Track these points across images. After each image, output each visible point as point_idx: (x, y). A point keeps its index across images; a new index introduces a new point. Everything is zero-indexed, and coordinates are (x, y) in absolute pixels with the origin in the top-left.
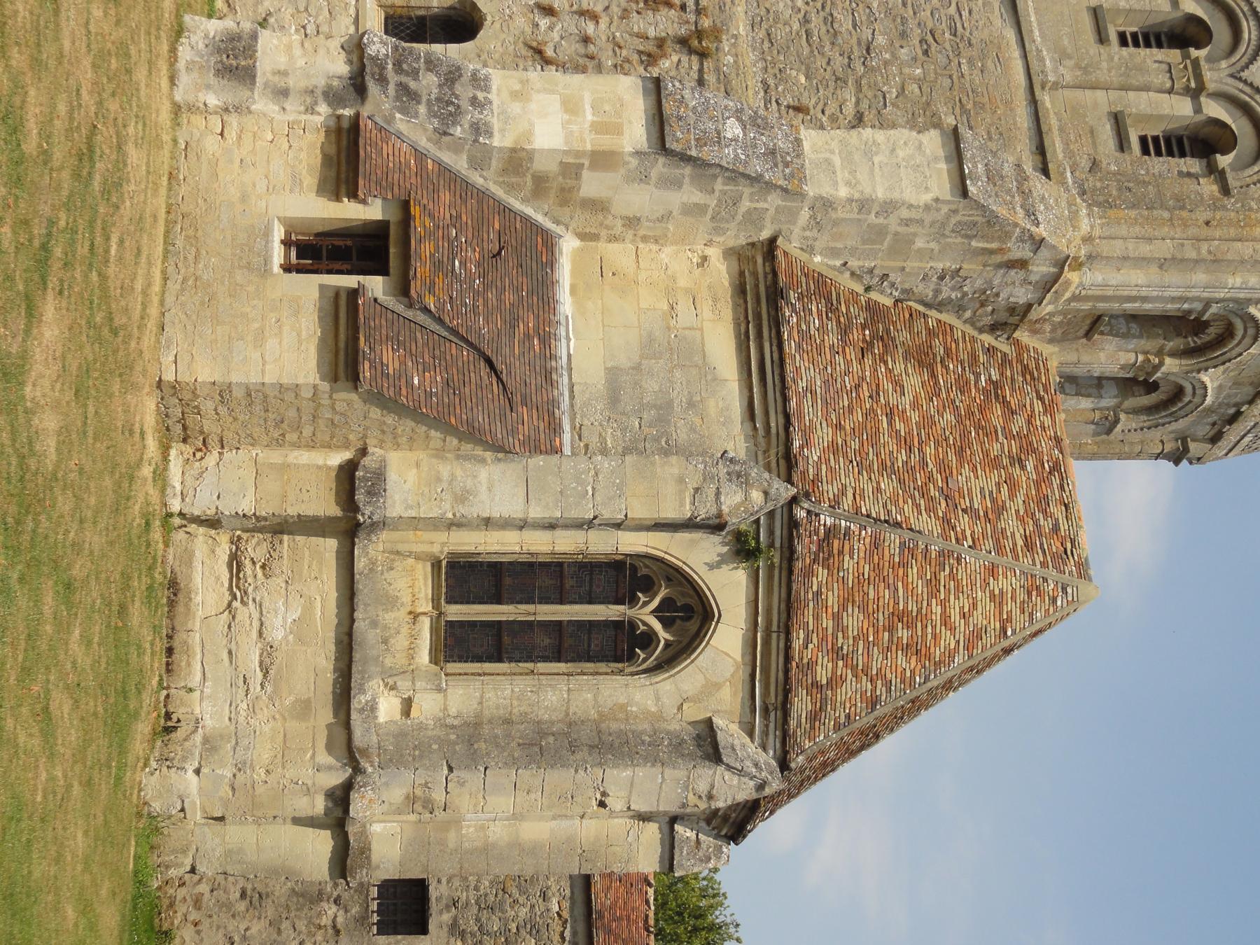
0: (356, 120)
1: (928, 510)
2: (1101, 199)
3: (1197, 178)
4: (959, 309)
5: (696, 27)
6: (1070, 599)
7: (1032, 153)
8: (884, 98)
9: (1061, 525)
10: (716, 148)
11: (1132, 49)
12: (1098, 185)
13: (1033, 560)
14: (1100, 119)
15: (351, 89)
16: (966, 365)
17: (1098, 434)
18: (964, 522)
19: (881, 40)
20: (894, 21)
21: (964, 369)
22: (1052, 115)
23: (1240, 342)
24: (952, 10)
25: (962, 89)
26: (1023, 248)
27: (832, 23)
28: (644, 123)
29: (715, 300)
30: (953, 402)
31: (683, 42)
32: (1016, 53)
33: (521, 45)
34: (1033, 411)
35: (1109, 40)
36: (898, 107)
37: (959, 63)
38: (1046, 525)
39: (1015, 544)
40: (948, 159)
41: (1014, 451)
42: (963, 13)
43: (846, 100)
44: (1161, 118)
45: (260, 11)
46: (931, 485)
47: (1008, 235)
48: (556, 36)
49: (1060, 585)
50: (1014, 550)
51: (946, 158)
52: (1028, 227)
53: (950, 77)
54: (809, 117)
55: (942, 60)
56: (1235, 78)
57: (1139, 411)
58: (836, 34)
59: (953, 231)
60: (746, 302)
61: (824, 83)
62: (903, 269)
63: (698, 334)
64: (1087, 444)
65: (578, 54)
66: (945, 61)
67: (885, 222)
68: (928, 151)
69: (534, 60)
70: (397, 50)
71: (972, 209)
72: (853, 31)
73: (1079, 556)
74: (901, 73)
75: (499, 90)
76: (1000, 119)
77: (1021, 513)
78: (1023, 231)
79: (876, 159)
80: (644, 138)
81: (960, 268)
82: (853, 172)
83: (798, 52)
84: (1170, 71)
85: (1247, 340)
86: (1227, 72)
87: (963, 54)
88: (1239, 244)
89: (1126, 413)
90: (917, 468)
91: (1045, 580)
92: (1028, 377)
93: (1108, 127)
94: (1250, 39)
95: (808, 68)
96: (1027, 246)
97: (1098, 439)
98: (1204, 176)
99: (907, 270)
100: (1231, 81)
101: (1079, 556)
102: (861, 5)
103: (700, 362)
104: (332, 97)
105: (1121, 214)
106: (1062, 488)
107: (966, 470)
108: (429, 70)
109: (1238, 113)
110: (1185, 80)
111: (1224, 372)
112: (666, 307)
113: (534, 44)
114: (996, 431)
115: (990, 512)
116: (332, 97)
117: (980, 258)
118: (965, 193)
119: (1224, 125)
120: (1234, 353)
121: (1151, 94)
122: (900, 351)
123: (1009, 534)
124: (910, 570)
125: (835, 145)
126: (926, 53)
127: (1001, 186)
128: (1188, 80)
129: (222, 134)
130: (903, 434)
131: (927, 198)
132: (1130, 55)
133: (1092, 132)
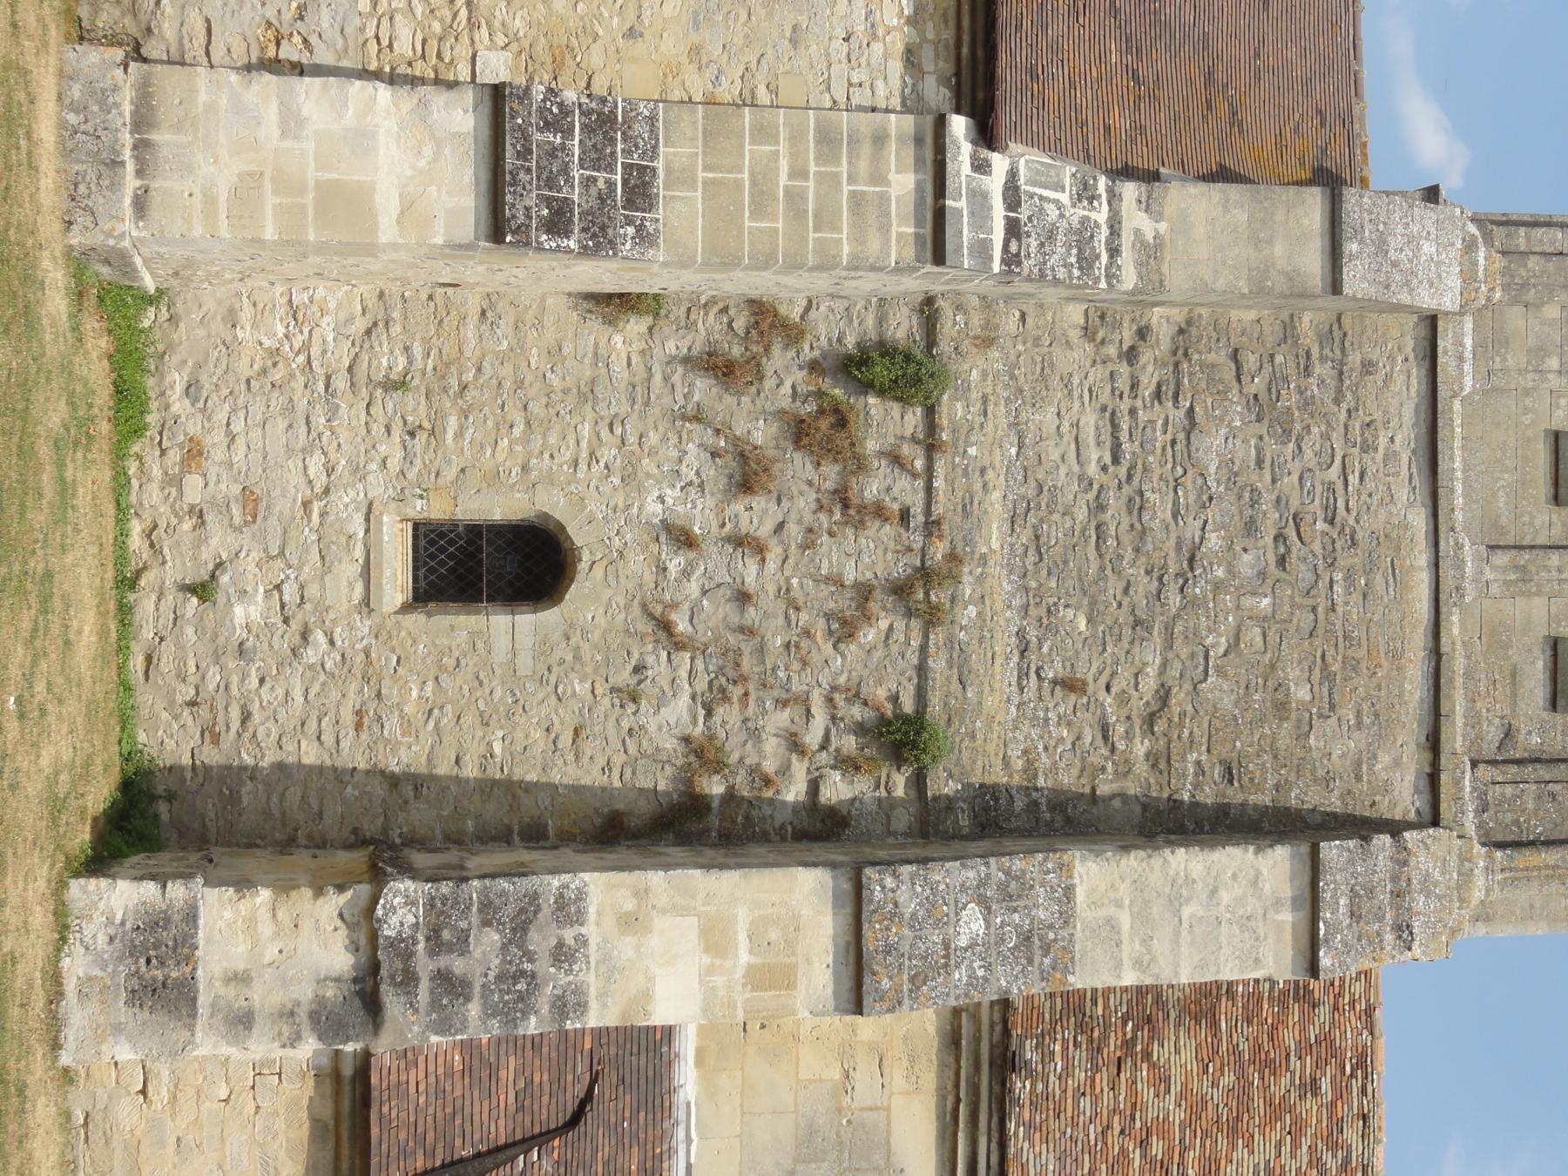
0: (364, 1063)
5: (923, 562)
8: (1207, 657)
10: (941, 980)
14: (1530, 650)
15: (357, 1002)
19: (1214, 541)
20: (1240, 497)
27: (1141, 508)
28: (830, 960)
29: (912, 1060)
31: (900, 590)
32: (1423, 559)
33: (636, 610)
37: (1331, 580)
40: (1296, 903)
42: (1350, 478)
43: (1145, 664)
45: (204, 556)
48: (693, 588)
51: (1294, 900)
54: (1085, 700)
55: (1304, 574)
58: (1144, 532)
60: (958, 1060)
61: (1116, 631)
63: (883, 1114)
65: (728, 627)
66: (1310, 576)
68: (1267, 887)
69: (657, 641)
70: (433, 906)
72: (1172, 526)
74: (1238, 607)
75: (599, 914)
76: (1379, 687)
79: (1186, 912)
80: (830, 991)
82: (1147, 941)
83: (1080, 570)
87: (1341, 562)
93: (1540, 664)
95: (1093, 603)
102: (1190, 473)
103: (882, 1163)
104: (326, 1022)
106: (1364, 1091)
108: (486, 923)
112: (837, 1075)
113: (658, 610)
116: (326, 1022)
125: (1125, 890)
126: (1282, 562)
129: (144, 1092)
133: (1514, 674)
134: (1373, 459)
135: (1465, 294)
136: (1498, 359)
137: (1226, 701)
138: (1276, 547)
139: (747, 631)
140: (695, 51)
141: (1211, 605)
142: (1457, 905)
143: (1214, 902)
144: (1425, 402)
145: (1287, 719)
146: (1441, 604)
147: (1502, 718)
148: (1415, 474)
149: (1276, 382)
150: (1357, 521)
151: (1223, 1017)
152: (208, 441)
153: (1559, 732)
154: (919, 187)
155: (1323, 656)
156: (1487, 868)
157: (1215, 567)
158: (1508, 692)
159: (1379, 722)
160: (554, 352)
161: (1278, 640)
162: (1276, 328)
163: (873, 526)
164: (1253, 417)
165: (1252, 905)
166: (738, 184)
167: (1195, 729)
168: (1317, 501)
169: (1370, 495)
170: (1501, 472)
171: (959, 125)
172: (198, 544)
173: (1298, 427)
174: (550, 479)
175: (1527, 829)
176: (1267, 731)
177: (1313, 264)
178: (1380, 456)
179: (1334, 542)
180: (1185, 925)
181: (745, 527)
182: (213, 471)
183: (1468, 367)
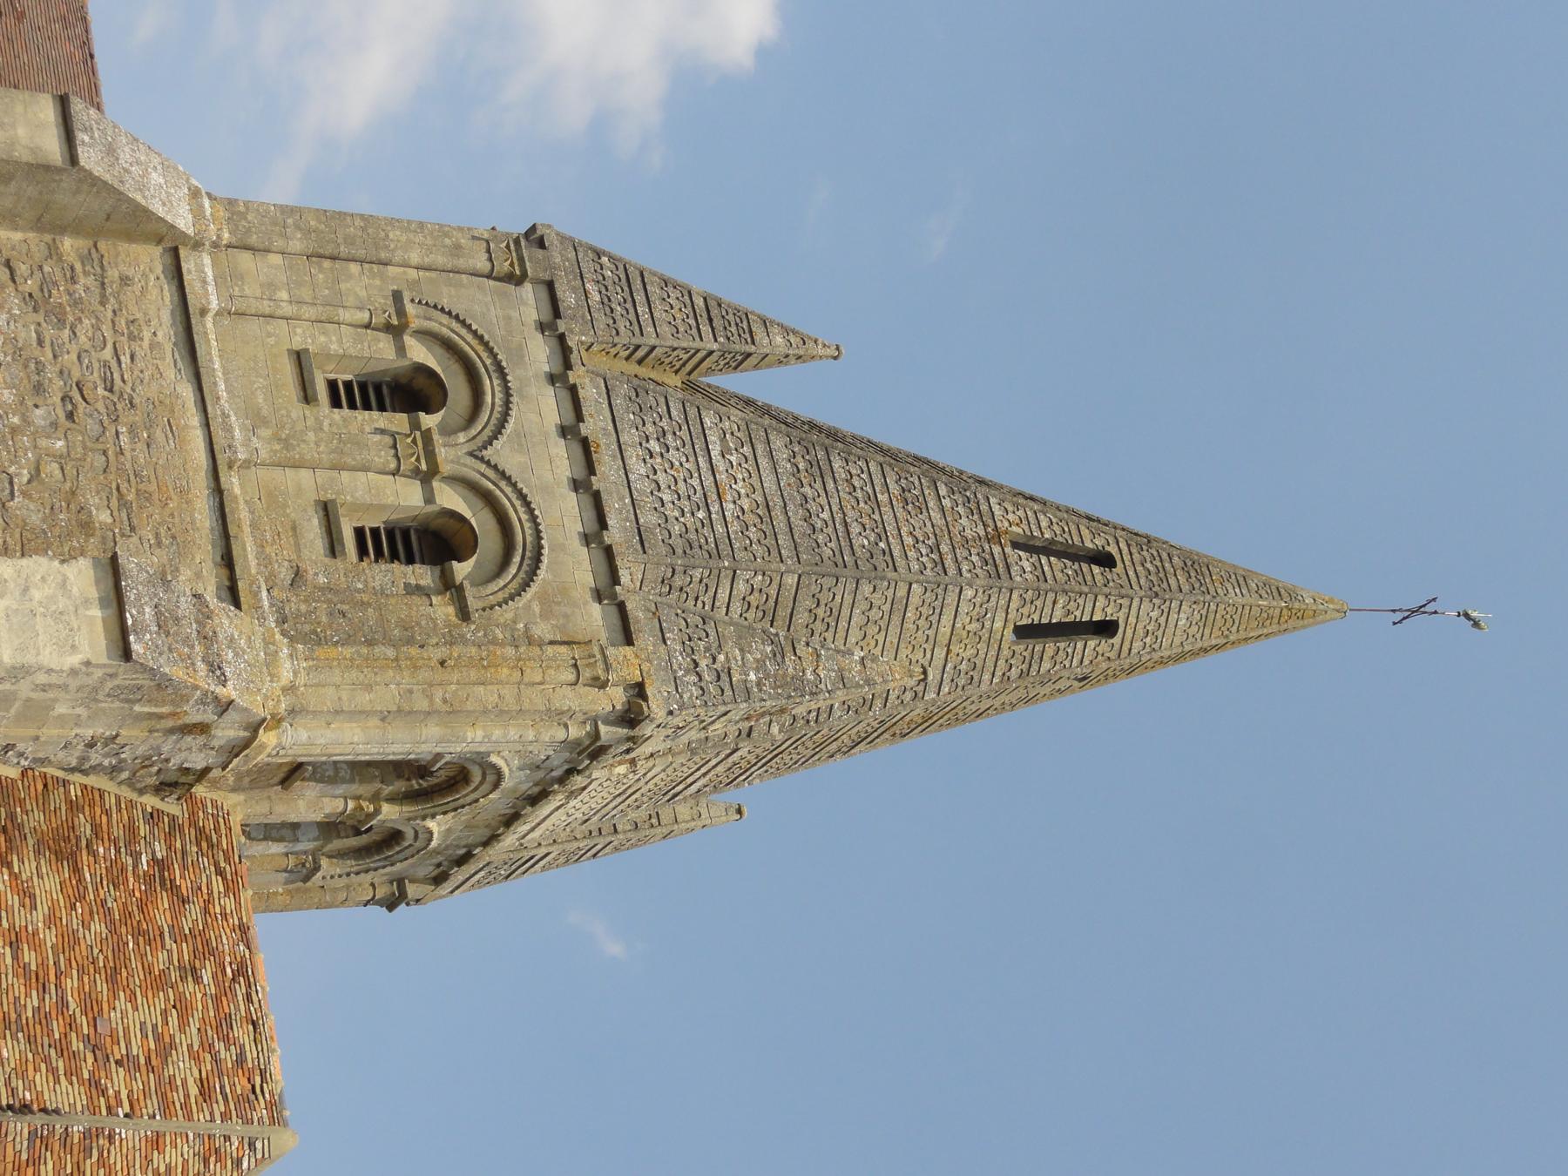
1: (69, 1074)
2: (307, 628)
3: (428, 596)
4: (113, 771)
6: (259, 1156)
7: (216, 564)
8: (11, 483)
9: (248, 1054)
11: (346, 411)
12: (303, 608)
13: (212, 1114)
14: (305, 510)
16: (122, 844)
17: (293, 882)
18: (118, 1081)
20: (26, 367)
21: (118, 851)
22: (242, 505)
23: (476, 789)
24: (108, 354)
25: (121, 470)
26: (205, 711)
30: (104, 903)
32: (195, 420)
34: (210, 893)
35: (317, 400)
36: (30, 497)
38: (228, 1056)
39: (187, 1096)
40: (103, 603)
41: (186, 958)
42: (122, 358)
44: (383, 507)
46: (74, 1035)
47: (185, 699)
49: (246, 1141)
50: (185, 1106)
51: (101, 600)
52: (212, 688)
53: (105, 453)
55: (92, 427)
56: (476, 457)
57: (345, 854)
59: (109, 695)
62: (37, 738)
64: (275, 894)
66: (97, 427)
67: (13, 688)
68: (75, 590)
71: (136, 672)
73: (271, 1093)
74: (35, 447)
76: (172, 515)
77: (196, 1048)
78: (205, 693)
81: (117, 735)
84: (395, 446)
85: (486, 787)
86: (467, 448)
88: (481, 688)
89: (330, 857)
90: (54, 1016)
91: (227, 1138)
92: (204, 845)
93: (315, 522)
94: (493, 404)
96: (210, 709)
97: (291, 887)
98: (439, 593)
99: (42, 739)
100: (470, 461)
101: (271, 1093)
105: (333, 652)
106: (249, 998)
107: (122, 1002)
109: (480, 504)
110: (413, 459)
111: (453, 818)
114: (162, 934)
115: (153, 1056)
117: (145, 724)
118: (127, 654)
119: (462, 519)
120: (469, 799)
121: (370, 475)
122: (31, 842)
123: (179, 1083)
124: (42, 1167)
126: (70, 416)
127: (176, 634)
128: (418, 460)
130: (33, 967)
131: (74, 660)
132: (345, 420)
133: (294, 528)
134: (140, 346)
135: (197, 226)
136: (237, 289)
137: (34, 518)
138: (64, 405)
141: (10, 443)
142: (269, 678)
143: (27, 598)
144: (178, 309)
145: (92, 535)
146: (216, 453)
147: (290, 561)
148: (179, 360)
149: (46, 284)
150: (134, 390)
151: (86, 868)
153: (342, 575)
155: (118, 489)
156: (291, 655)
157: (11, 416)
158: (292, 542)
159: (176, 541)
161: (75, 473)
162: (43, 248)
164: (31, 309)
165: (62, 603)
167: (8, 539)
168: (96, 374)
169: (142, 372)
170: (257, 377)
173: (71, 318)
175: (325, 637)
176: (75, 543)
177: (52, 147)
178: (146, 343)
179: (115, 404)
183: (211, 288)
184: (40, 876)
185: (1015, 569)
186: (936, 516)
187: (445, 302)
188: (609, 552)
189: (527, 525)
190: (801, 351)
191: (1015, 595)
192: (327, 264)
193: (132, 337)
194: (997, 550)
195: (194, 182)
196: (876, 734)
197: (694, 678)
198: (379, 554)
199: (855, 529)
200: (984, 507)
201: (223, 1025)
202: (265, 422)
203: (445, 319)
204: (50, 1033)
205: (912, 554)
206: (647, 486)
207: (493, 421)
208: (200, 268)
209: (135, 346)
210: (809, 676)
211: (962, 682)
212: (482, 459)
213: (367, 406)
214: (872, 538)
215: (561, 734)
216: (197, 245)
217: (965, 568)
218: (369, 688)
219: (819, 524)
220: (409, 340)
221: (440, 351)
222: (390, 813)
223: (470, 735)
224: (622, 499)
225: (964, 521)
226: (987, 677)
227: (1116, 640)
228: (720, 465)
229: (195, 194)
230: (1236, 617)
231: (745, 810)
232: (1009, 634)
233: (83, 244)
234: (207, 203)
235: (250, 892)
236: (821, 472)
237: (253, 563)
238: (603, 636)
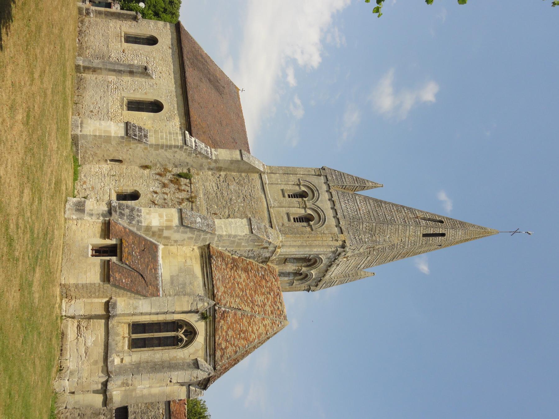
11: (291, 198)
18: (256, 308)
21: (256, 272)
24: (250, 191)
25: (253, 208)
29: (196, 259)
30: (253, 280)
32: (265, 200)
34: (272, 281)
38: (276, 308)
39: (269, 313)
48: (158, 198)
50: (268, 314)
55: (248, 202)
62: (240, 250)
78: (266, 240)
79: (232, 226)
82: (227, 229)
85: (320, 263)
91: (276, 321)
95: (217, 205)
96: (267, 244)
97: (290, 287)
98: (307, 227)
105: (288, 236)
106: (280, 299)
109: (315, 212)
112: (184, 261)
116: (104, 215)
118: (252, 233)
120: (318, 266)
126: (244, 200)
131: (244, 234)
139: (166, 203)
140: (153, 127)
149: (240, 181)
152: (87, 181)
154: (182, 138)
160: (137, 173)
163: (183, 192)
166: (159, 137)
171: (187, 132)
172: (85, 193)
174: (136, 186)
177: (239, 158)
180: (232, 227)
181: (165, 192)
182: (87, 185)
184: (242, 274)
185: (421, 223)
186: (404, 214)
187: (307, 180)
188: (338, 219)
189: (323, 215)
190: (375, 186)
191: (422, 228)
192: (287, 175)
193: (254, 188)
194: (417, 220)
195: (263, 163)
196: (397, 256)
197: (355, 240)
198: (298, 222)
199: (387, 216)
200: (414, 212)
201: (275, 303)
202: (277, 200)
203: (307, 183)
204: (244, 299)
205: (399, 220)
206: (345, 208)
207: (317, 199)
208: (265, 177)
209: (254, 189)
210: (378, 240)
211: (413, 245)
212: (314, 205)
213: (295, 197)
214: (391, 217)
215: (331, 250)
216: (264, 173)
217: (410, 223)
218: (295, 241)
219: (380, 215)
220: (301, 186)
221: (307, 188)
222: (304, 269)
223: (314, 250)
224: (341, 210)
225: (410, 215)
226: (418, 244)
227: (445, 237)
228: (360, 205)
229: (264, 165)
230: (473, 233)
231: (375, 274)
232: (421, 235)
233: (245, 174)
234: (266, 166)
235: (280, 282)
236: (380, 206)
237: (275, 223)
238: (338, 233)
